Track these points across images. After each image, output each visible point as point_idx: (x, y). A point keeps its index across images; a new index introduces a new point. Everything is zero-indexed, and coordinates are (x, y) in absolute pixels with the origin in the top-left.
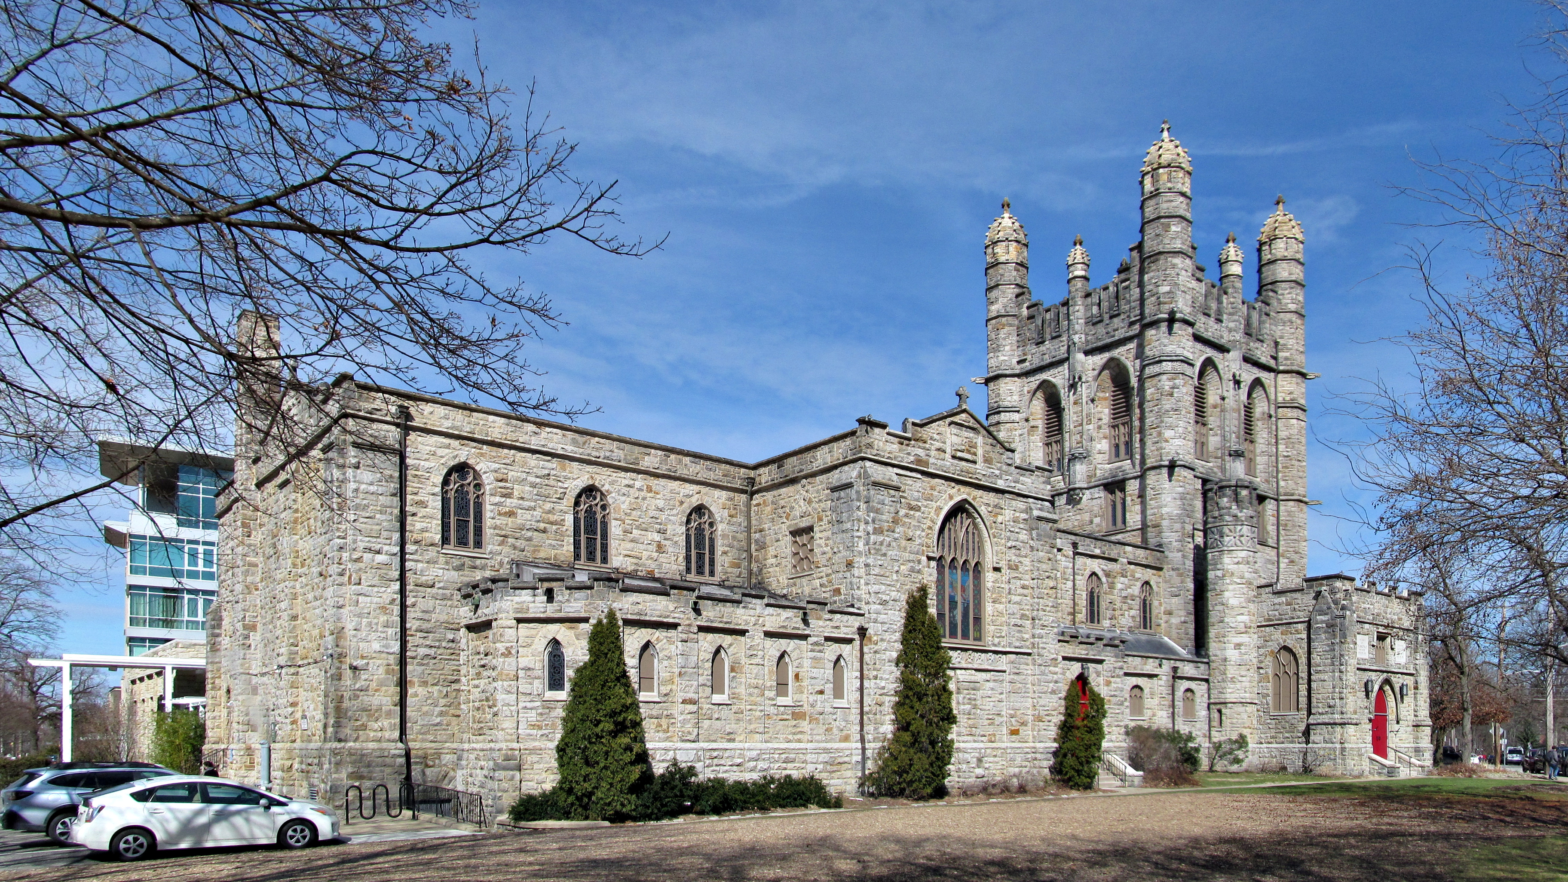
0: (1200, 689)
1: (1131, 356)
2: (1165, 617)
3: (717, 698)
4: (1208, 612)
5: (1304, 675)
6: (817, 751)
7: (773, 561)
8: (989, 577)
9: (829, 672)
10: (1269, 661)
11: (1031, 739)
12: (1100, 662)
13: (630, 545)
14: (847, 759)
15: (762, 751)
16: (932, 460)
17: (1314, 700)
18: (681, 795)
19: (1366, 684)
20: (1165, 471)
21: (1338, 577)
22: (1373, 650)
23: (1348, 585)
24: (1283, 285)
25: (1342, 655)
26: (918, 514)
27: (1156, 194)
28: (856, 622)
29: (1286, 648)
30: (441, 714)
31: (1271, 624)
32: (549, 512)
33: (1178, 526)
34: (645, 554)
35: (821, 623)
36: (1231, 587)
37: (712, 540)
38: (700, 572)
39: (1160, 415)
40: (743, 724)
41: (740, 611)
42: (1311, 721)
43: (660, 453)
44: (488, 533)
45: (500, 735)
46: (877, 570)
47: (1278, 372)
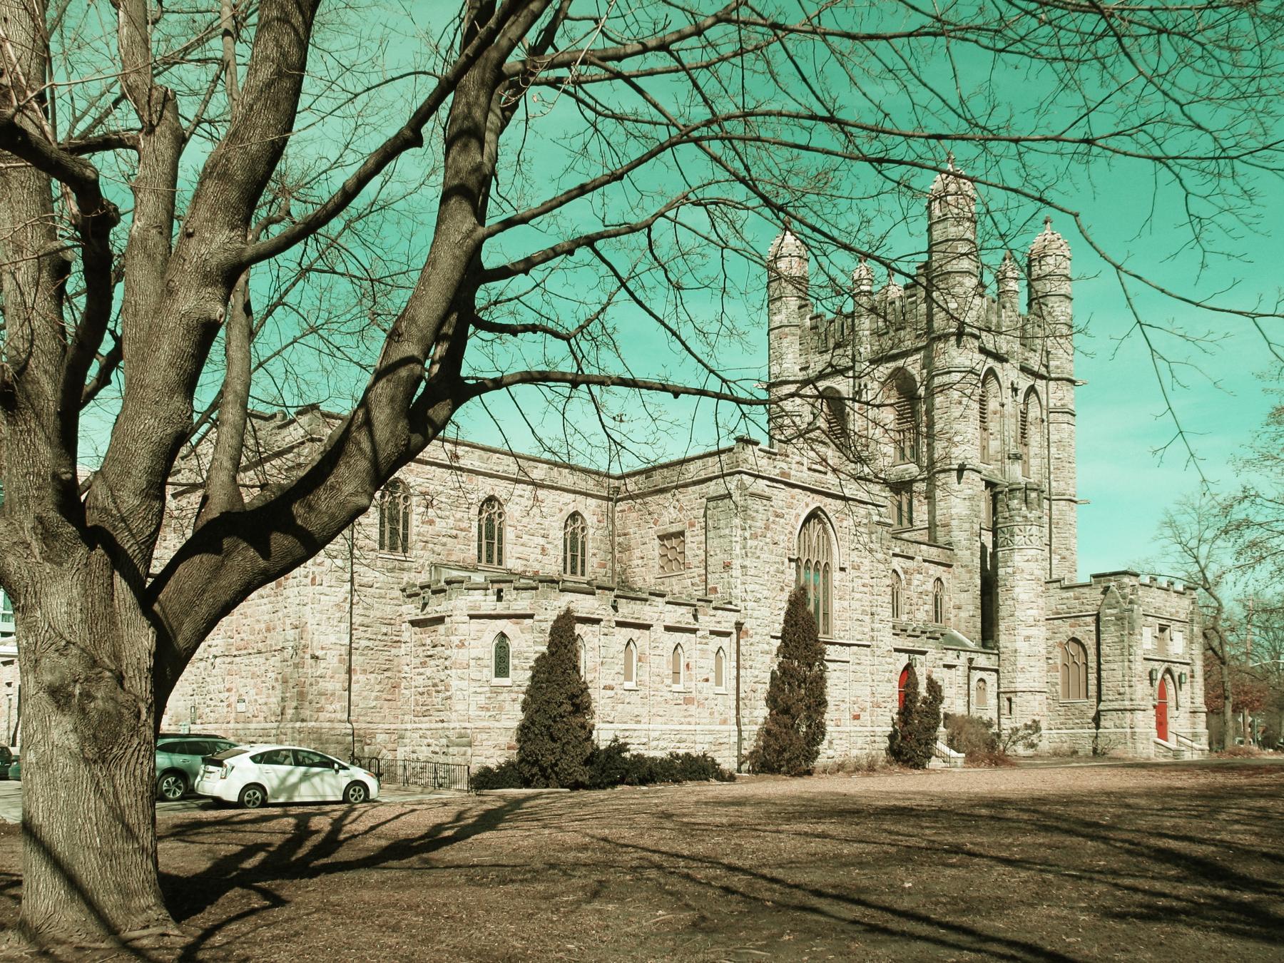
0: (991, 678)
1: (918, 366)
2: (954, 612)
4: (998, 606)
5: (1093, 664)
6: (704, 732)
7: (640, 562)
8: (836, 576)
10: (1058, 654)
11: (869, 724)
12: (924, 653)
14: (726, 740)
16: (793, 473)
17: (1104, 688)
18: (616, 768)
19: (1151, 673)
20: (954, 474)
21: (1125, 573)
23: (1134, 581)
24: (1053, 299)
26: (782, 520)
28: (734, 617)
29: (1074, 640)
30: (377, 698)
31: (1058, 617)
32: (460, 520)
33: (966, 526)
36: (1021, 583)
37: (583, 543)
38: (574, 572)
41: (647, 608)
42: (1101, 707)
43: (546, 466)
44: (413, 537)
46: (752, 572)
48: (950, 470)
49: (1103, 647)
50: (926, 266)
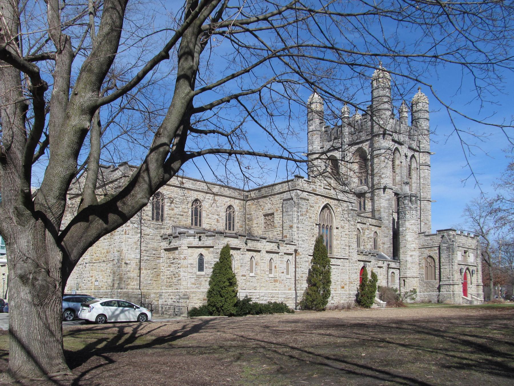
0: (397, 272)
1: (367, 147)
2: (382, 245)
3: (251, 274)
5: (437, 266)
7: (256, 225)
8: (335, 231)
9: (285, 265)
10: (423, 261)
12: (370, 262)
13: (209, 220)
15: (265, 293)
16: (317, 189)
17: (442, 276)
18: (246, 308)
19: (461, 270)
20: (382, 190)
21: (450, 230)
22: (463, 257)
23: (454, 233)
24: (421, 120)
25: (452, 259)
28: (294, 247)
29: (430, 256)
30: (151, 280)
32: (184, 208)
33: (387, 211)
34: (213, 223)
35: (283, 248)
36: (409, 234)
37: (233, 218)
39: (380, 169)
40: (259, 284)
41: (259, 244)
42: (441, 283)
43: (218, 187)
44: (165, 215)
45: (182, 287)
46: (301, 229)
47: (420, 152)
48: (380, 188)
50: (371, 106)
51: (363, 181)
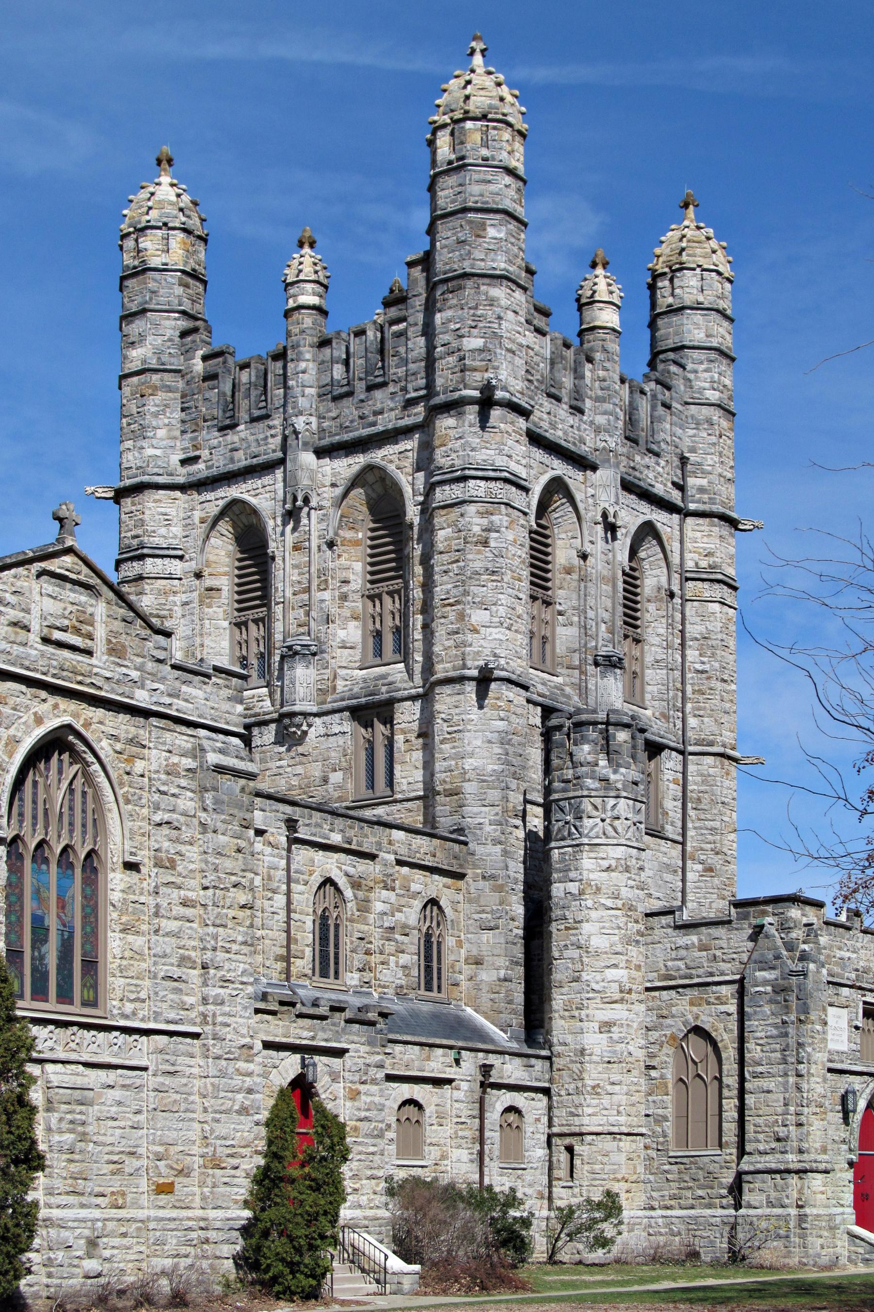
0: (533, 1107)
5: (731, 1081)
8: (116, 882)
10: (667, 1056)
12: (340, 1053)
17: (750, 1128)
19: (844, 1099)
20: (470, 688)
22: (857, 1036)
23: (812, 915)
24: (695, 354)
25: (800, 1045)
27: (458, 166)
29: (698, 1031)
31: (670, 985)
33: (494, 795)
36: (594, 914)
39: (463, 580)
42: (745, 1167)
48: (462, 679)
49: (750, 1045)
50: (427, 261)
51: (390, 641)
